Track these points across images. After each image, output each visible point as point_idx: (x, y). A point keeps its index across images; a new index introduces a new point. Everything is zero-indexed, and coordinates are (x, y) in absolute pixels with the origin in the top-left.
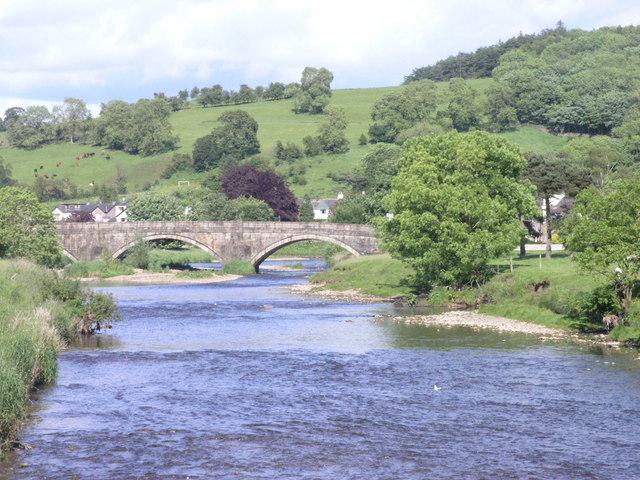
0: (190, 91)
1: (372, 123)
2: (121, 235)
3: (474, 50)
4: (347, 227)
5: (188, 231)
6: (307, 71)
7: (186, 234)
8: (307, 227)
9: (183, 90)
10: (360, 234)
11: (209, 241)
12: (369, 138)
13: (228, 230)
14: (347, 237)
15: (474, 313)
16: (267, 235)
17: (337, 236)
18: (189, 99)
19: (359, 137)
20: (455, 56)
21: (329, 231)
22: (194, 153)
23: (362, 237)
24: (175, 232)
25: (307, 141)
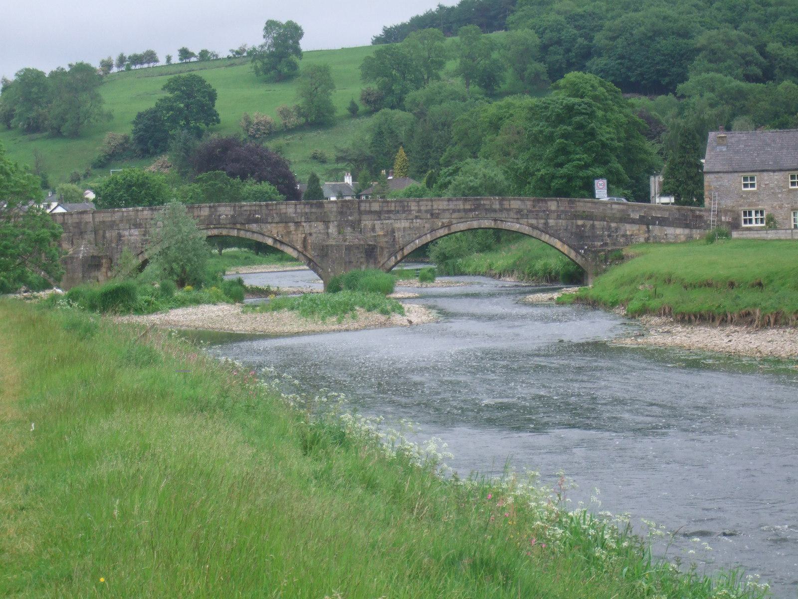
0: (115, 60)
1: (364, 88)
2: (135, 232)
3: (399, 24)
4: (553, 205)
5: (257, 221)
6: (271, 25)
7: (254, 227)
8: (477, 208)
9: (106, 59)
10: (576, 216)
11: (298, 238)
12: (362, 108)
13: (332, 218)
14: (551, 222)
15: (772, 333)
16: (404, 224)
17: (534, 222)
18: (115, 70)
19: (348, 105)
20: (434, 10)
21: (519, 211)
22: (135, 132)
23: (580, 222)
24: (233, 222)
25: (285, 113)
